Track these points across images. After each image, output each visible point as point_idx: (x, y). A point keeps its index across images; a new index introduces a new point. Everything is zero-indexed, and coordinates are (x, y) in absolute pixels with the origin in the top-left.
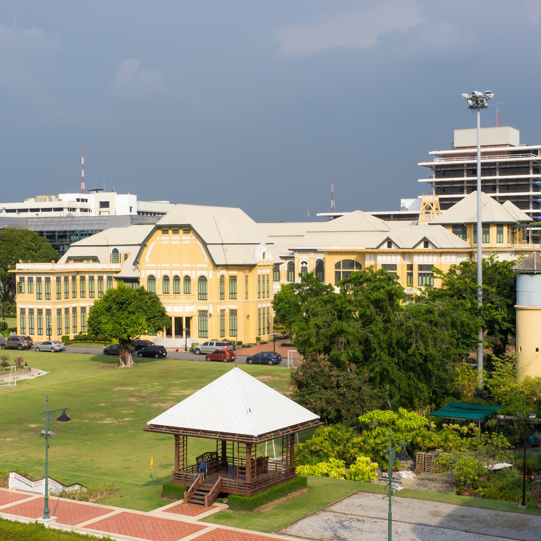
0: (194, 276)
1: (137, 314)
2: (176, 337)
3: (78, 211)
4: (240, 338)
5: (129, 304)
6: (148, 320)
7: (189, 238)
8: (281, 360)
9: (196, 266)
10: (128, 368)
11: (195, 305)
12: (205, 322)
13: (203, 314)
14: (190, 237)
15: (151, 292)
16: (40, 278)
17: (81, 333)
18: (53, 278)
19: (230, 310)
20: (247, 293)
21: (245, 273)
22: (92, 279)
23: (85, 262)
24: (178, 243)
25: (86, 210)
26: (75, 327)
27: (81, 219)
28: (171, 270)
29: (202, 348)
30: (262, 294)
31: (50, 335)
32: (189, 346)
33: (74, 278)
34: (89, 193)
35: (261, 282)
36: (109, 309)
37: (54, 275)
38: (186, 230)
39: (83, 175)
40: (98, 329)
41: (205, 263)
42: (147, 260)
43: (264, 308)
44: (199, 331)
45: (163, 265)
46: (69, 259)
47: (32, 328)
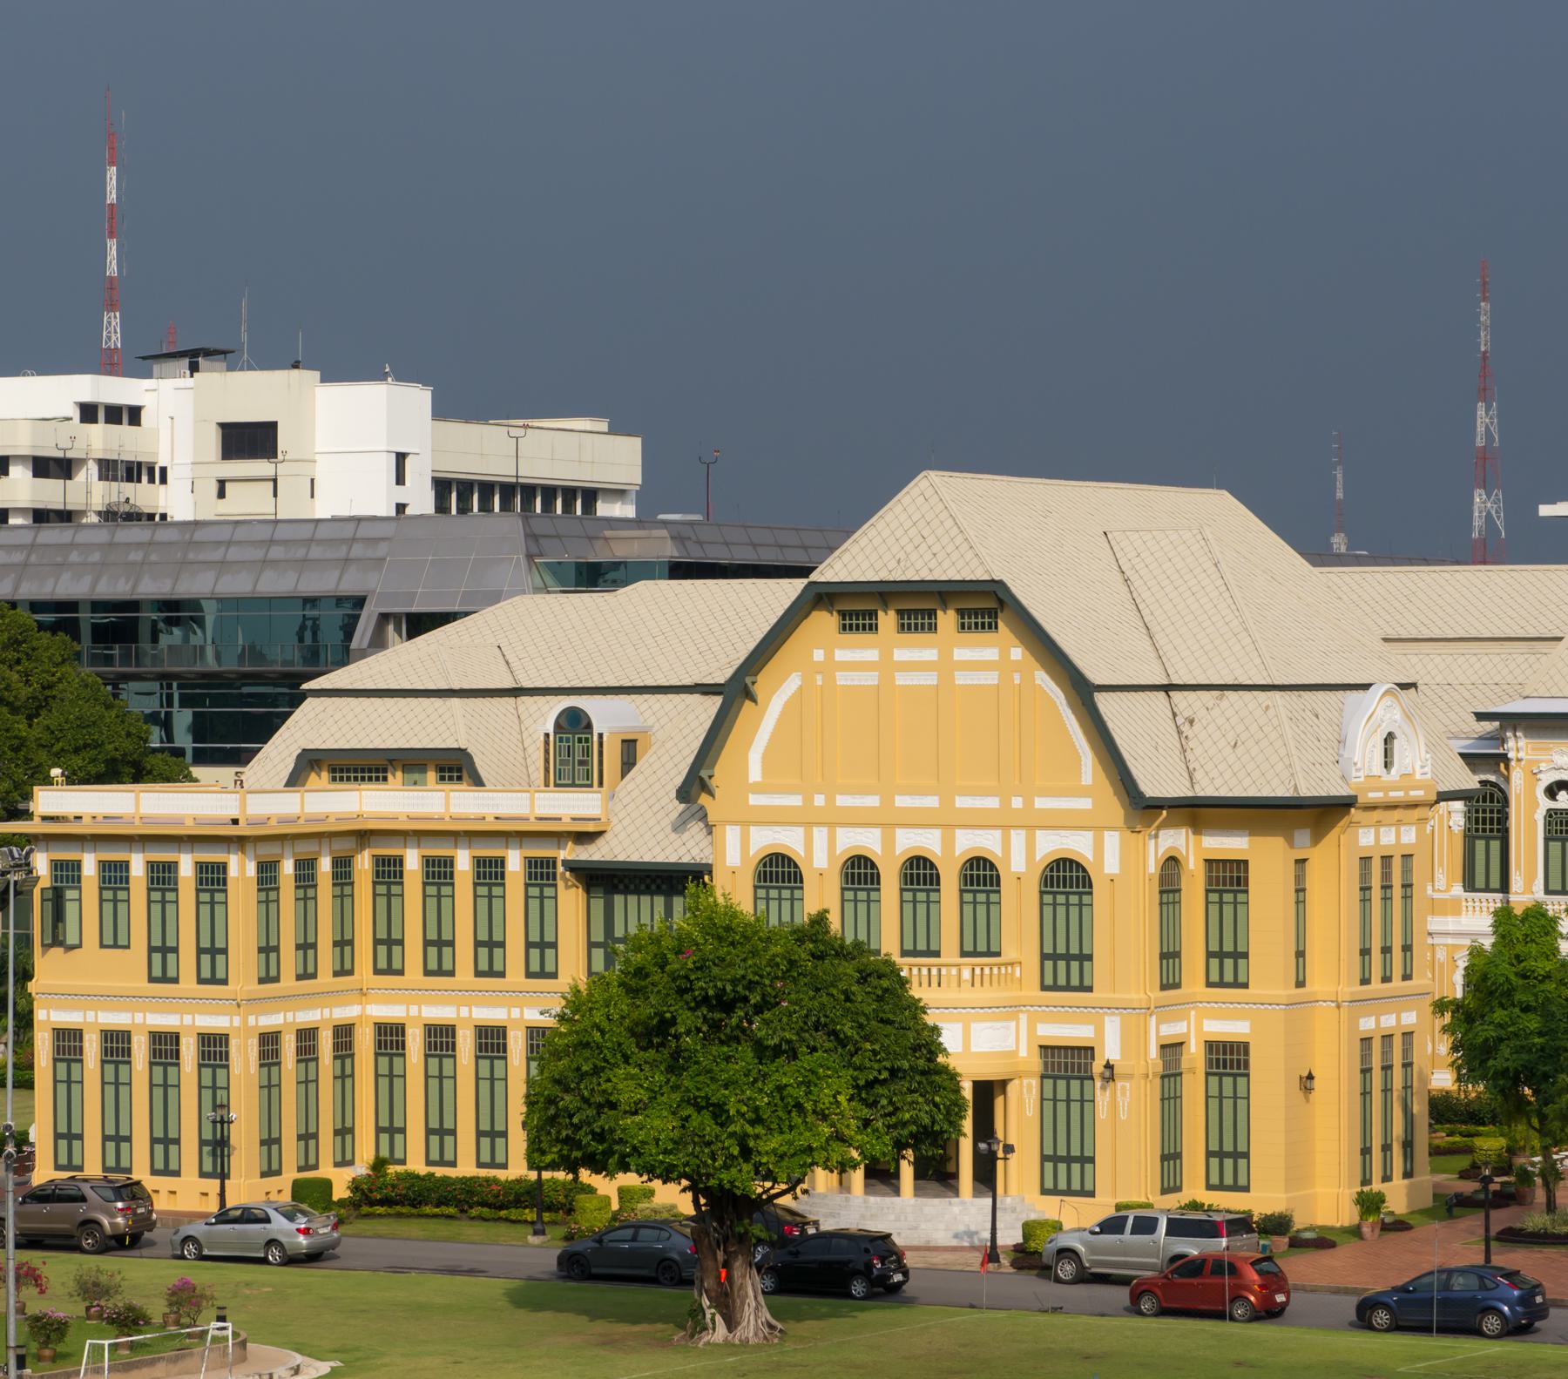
0: (1021, 861)
1: (806, 1060)
2: (918, 1192)
3: (88, 475)
4: (1261, 1201)
5: (759, 1010)
6: (864, 1092)
7: (991, 654)
8: (1541, 1313)
9: (1029, 803)
10: (745, 1343)
11: (1023, 1018)
12: (1075, 1107)
13: (1068, 1067)
14: (988, 657)
15: (857, 944)
16: (172, 867)
17: (379, 1165)
18: (241, 869)
19: (1212, 1046)
20: (1300, 954)
21: (1291, 844)
22: (439, 872)
23: (396, 778)
24: (930, 679)
25: (133, 471)
26: (344, 1132)
27: (241, 534)
28: (888, 824)
29: (1092, 1249)
30: (1385, 954)
31: (223, 1176)
32: (1010, 1236)
33: (343, 871)
34: (148, 375)
35: (1376, 893)
36: (656, 1032)
37: (249, 848)
38: (976, 612)
39: (112, 269)
40: (600, 1137)
41: (1083, 792)
42: (755, 774)
43: (1387, 1038)
44: (1044, 1158)
45: (842, 801)
46: (309, 762)
47: (165, 1141)
